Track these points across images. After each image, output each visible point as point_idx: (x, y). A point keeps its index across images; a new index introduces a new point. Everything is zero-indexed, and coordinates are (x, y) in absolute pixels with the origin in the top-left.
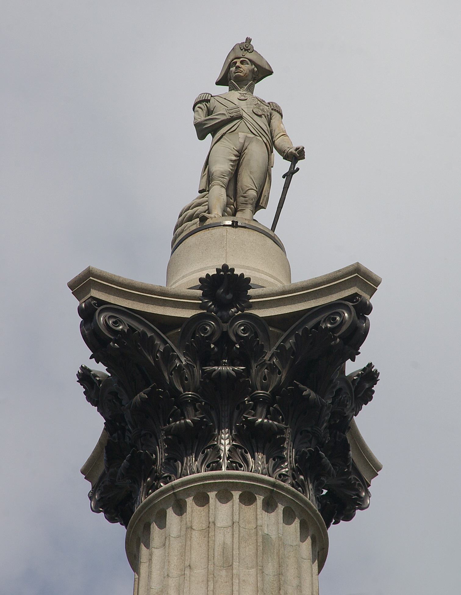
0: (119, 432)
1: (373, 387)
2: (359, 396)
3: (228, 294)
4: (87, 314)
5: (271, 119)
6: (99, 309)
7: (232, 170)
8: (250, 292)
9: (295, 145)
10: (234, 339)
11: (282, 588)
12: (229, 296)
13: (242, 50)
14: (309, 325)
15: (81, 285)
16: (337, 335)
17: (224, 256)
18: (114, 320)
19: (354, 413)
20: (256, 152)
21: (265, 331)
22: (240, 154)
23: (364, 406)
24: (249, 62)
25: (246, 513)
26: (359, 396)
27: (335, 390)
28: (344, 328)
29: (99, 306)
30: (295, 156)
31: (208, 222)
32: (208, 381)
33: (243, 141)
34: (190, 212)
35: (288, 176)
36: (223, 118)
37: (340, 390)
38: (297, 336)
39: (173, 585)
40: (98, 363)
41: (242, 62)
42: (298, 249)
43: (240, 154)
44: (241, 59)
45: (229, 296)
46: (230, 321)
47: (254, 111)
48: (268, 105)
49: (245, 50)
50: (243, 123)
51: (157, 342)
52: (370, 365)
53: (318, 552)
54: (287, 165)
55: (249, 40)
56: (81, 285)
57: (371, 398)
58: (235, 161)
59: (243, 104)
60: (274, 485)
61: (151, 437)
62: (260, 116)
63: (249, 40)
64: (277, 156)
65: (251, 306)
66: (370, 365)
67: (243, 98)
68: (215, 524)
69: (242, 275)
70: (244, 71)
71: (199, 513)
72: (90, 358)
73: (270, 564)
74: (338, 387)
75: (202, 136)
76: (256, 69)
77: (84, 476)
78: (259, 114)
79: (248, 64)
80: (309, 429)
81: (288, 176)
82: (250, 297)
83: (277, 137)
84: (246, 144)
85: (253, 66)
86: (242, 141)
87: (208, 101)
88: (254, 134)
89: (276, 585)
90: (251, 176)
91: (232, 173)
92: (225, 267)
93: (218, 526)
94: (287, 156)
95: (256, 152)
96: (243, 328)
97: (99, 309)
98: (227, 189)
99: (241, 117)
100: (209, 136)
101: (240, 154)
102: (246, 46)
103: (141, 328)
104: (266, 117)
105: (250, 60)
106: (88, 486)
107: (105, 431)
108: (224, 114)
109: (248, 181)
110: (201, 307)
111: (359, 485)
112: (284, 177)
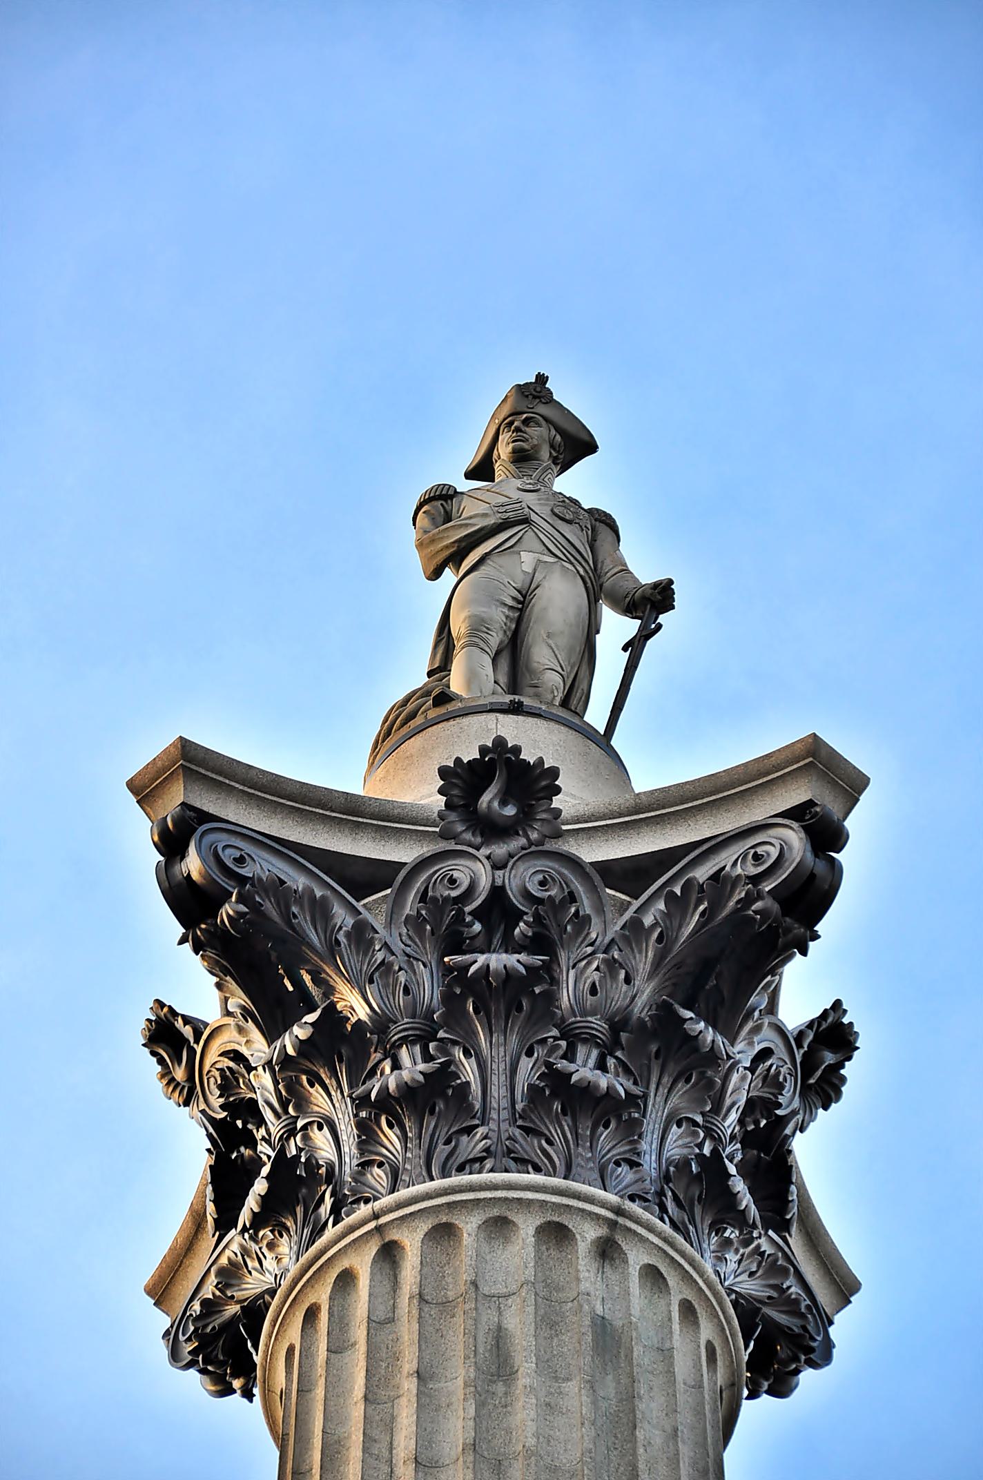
1: (843, 1067)
2: (812, 1081)
3: (504, 803)
7: (507, 617)
11: (639, 1425)
12: (510, 811)
15: (145, 790)
16: (767, 889)
20: (560, 596)
22: (523, 602)
24: (543, 423)
25: (551, 1269)
26: (812, 1081)
30: (652, 603)
32: (458, 991)
33: (530, 570)
35: (635, 647)
36: (480, 523)
41: (526, 422)
42: (671, 729)
43: (524, 597)
45: (510, 811)
47: (556, 510)
49: (535, 397)
50: (530, 533)
52: (671, 582)
54: (630, 627)
55: (541, 379)
59: (530, 499)
61: (320, 1128)
63: (541, 379)
65: (558, 835)
68: (477, 1287)
70: (543, 432)
71: (438, 1269)
72: (180, 943)
73: (610, 1377)
75: (435, 574)
76: (558, 438)
80: (699, 1119)
82: (557, 813)
83: (609, 575)
84: (538, 577)
85: (553, 432)
86: (528, 568)
88: (556, 556)
89: (625, 1420)
90: (550, 642)
94: (630, 608)
99: (526, 521)
108: (485, 515)
110: (445, 835)
112: (625, 649)
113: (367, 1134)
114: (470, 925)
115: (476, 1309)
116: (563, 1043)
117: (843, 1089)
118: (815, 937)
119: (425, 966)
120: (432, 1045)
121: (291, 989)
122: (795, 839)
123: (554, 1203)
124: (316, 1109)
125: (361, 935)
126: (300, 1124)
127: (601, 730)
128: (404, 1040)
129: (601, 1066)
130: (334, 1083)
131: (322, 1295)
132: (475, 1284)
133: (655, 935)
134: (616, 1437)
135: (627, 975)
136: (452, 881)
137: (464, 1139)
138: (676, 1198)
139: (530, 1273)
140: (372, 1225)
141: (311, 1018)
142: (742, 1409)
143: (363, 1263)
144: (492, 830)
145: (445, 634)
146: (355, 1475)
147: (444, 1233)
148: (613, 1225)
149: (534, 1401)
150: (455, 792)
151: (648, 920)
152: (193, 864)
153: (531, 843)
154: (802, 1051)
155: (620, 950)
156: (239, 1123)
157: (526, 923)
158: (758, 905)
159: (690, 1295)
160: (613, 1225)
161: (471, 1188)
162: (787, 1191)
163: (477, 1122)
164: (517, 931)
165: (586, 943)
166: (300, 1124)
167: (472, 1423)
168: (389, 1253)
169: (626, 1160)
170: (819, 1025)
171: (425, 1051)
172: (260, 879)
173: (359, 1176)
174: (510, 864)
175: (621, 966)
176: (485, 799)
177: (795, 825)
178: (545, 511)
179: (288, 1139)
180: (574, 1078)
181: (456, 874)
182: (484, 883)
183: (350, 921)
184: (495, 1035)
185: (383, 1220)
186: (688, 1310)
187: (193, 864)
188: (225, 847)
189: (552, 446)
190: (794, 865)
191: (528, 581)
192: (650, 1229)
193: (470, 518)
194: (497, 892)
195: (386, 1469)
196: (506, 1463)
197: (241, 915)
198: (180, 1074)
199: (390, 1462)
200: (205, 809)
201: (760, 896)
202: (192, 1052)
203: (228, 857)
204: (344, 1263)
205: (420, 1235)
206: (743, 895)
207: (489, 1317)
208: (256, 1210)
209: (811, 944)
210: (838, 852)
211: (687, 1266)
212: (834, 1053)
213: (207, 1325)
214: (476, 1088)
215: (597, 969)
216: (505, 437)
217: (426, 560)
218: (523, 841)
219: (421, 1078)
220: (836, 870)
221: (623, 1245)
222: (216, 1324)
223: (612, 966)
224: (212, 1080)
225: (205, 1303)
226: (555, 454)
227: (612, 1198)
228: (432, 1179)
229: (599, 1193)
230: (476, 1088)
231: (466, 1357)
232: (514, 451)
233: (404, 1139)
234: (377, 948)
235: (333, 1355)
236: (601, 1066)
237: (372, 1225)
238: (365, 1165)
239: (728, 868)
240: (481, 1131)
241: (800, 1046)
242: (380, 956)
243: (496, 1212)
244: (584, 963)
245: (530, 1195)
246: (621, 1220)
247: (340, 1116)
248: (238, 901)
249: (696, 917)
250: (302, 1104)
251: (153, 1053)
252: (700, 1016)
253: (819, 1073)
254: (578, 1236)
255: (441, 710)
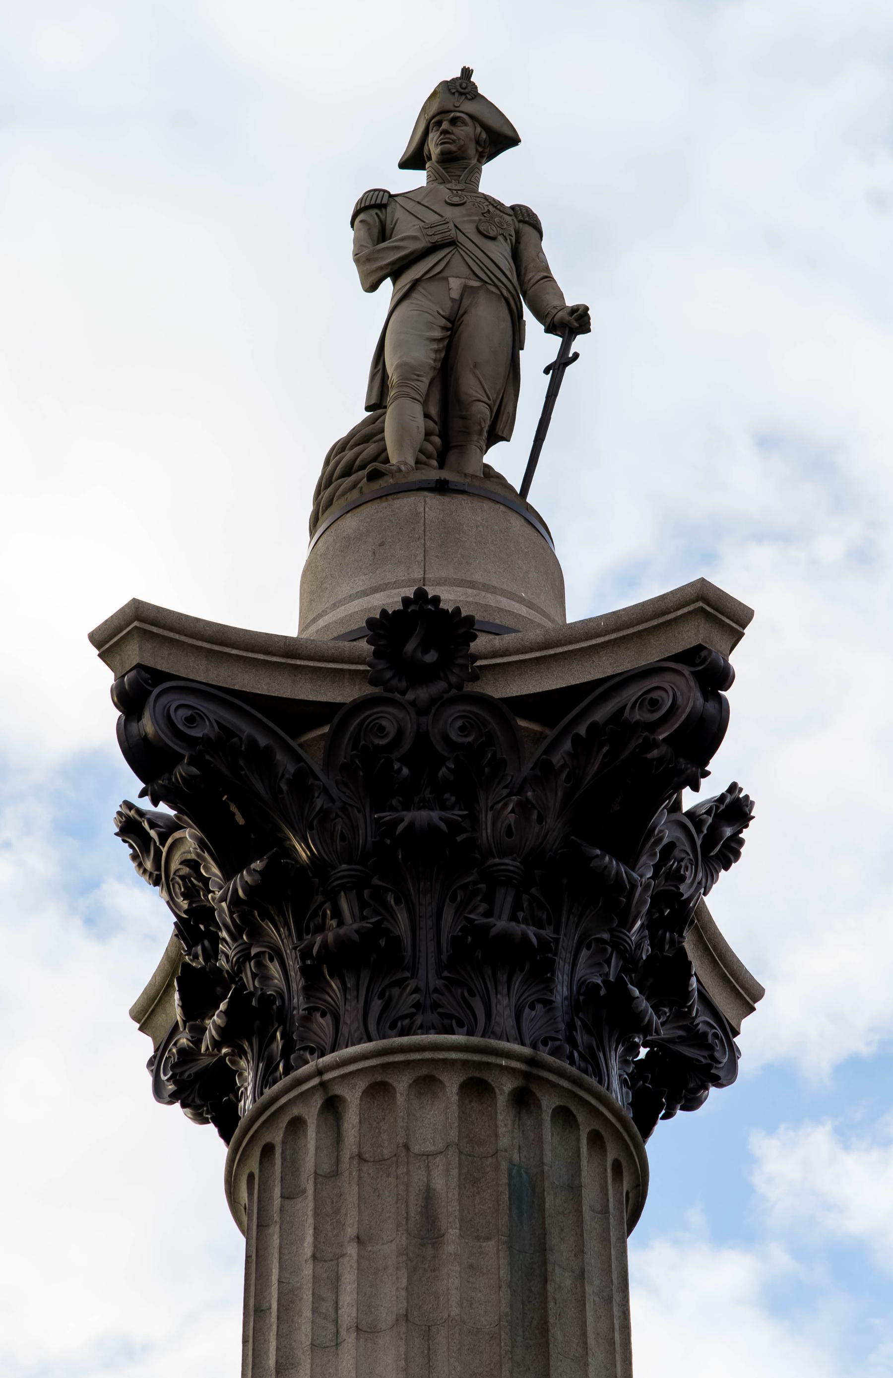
0: (206, 943)
3: (426, 651)
4: (129, 699)
5: (518, 241)
6: (156, 691)
7: (435, 360)
8: (481, 643)
9: (570, 302)
10: (440, 747)
12: (431, 657)
13: (454, 94)
14: (601, 714)
15: (108, 641)
16: (661, 737)
17: (420, 558)
18: (189, 713)
19: (702, 891)
21: (510, 729)
23: (722, 873)
27: (658, 850)
28: (406, 746)
29: (155, 686)
31: (527, 1010)
34: (349, 455)
35: (557, 370)
37: (671, 846)
38: (577, 738)
39: (325, 1276)
40: (754, 1009)
41: (454, 121)
44: (452, 115)
45: (431, 657)
46: (433, 711)
47: (481, 228)
48: (511, 212)
49: (461, 94)
50: (457, 256)
51: (279, 757)
53: (627, 1193)
55: (467, 73)
56: (108, 641)
57: (737, 855)
58: (439, 340)
60: (532, 1062)
62: (493, 239)
63: (467, 73)
64: (532, 325)
65: (475, 678)
66: (733, 788)
67: (456, 200)
69: (457, 610)
70: (462, 129)
71: (375, 1124)
74: (666, 841)
75: (372, 287)
76: (484, 136)
77: (138, 1025)
78: (492, 234)
79: (465, 124)
80: (606, 936)
81: (557, 370)
82: (475, 658)
83: (532, 282)
84: (466, 303)
85: (479, 129)
86: (455, 295)
87: (382, 207)
91: (435, 368)
92: (421, 594)
93: (416, 1151)
95: (486, 317)
96: (459, 723)
97: (156, 691)
98: (425, 403)
100: (387, 284)
101: (453, 326)
102: (462, 87)
103: (246, 729)
104: (506, 240)
105: (471, 116)
106: (146, 1046)
107: (175, 939)
108: (415, 238)
109: (474, 388)
110: (373, 682)
111: (716, 1035)
112: (546, 371)
113: (313, 983)
114: (400, 770)
115: (408, 1173)
116: (483, 886)
117: (741, 850)
118: (706, 774)
119: (359, 811)
120: (366, 893)
121: (241, 820)
122: (693, 699)
123: (474, 1062)
124: (267, 939)
125: (303, 782)
126: (254, 951)
127: (517, 484)
128: (344, 887)
129: (513, 918)
130: (282, 919)
131: (277, 1136)
132: (407, 1147)
133: (564, 776)
134: (530, 1291)
135: (539, 814)
136: (382, 729)
137: (396, 991)
138: (585, 1026)
139: (454, 1135)
140: (315, 1081)
141: (257, 865)
142: (656, 1128)
143: (311, 1112)
144: (419, 675)
145: (380, 366)
146: (306, 1335)
147: (379, 1090)
148: (527, 1076)
149: (458, 1268)
150: (382, 642)
151: (557, 759)
152: (148, 725)
153: (451, 686)
154: (702, 836)
155: (534, 791)
156: (202, 927)
157: (448, 768)
158: (655, 753)
159: (596, 1125)
160: (527, 1076)
161: (402, 1049)
162: (687, 983)
163: (407, 974)
164: (441, 773)
165: (502, 785)
166: (254, 951)
167: (403, 1293)
168: (333, 1106)
169: (539, 1001)
170: (717, 807)
171: (360, 897)
172: (209, 739)
173: (307, 1018)
174: (433, 711)
175: (534, 807)
176: (411, 647)
177: (686, 670)
178: (470, 229)
179: (244, 963)
180: (493, 931)
181: (384, 723)
182: (410, 729)
183: (291, 768)
184: (422, 884)
185: (327, 1076)
186: (596, 1139)
187: (148, 725)
188: (179, 707)
189: (478, 142)
190: (684, 717)
191: (456, 307)
192: (560, 1073)
193: (402, 239)
194: (422, 737)
195: (333, 1329)
196: (434, 1329)
197: (193, 777)
198: (149, 865)
199: (336, 1322)
200: (159, 668)
201: (655, 744)
202: (158, 853)
203: (179, 718)
204: (295, 1111)
205: (358, 1093)
206: (640, 741)
207: (418, 1177)
208: (493, 931)
209: (702, 780)
210: (726, 690)
211: (594, 1102)
212: (729, 826)
213: (184, 1072)
214: (407, 941)
215: (512, 811)
216: (433, 137)
217: (364, 276)
218: (442, 685)
219: (356, 937)
220: (723, 708)
221: (538, 1094)
222: (193, 1071)
223: (524, 808)
224: (177, 886)
225: (181, 1051)
226: (480, 150)
227: (527, 1051)
228: (370, 1040)
229: (516, 1047)
230: (407, 941)
231: (399, 1225)
232: (443, 153)
233: (345, 989)
234: (316, 795)
235: (287, 1202)
236: (513, 918)
237: (315, 1081)
238: (311, 1010)
239: (627, 713)
240: (412, 984)
241: (699, 831)
242: (319, 803)
243: (424, 1071)
244: (501, 804)
245: (454, 1055)
246: (535, 1071)
247: (288, 951)
248: (190, 763)
249: (600, 758)
250: (256, 934)
251: (124, 841)
252: (606, 850)
253: (719, 847)
254: (497, 1090)
255: (377, 485)
